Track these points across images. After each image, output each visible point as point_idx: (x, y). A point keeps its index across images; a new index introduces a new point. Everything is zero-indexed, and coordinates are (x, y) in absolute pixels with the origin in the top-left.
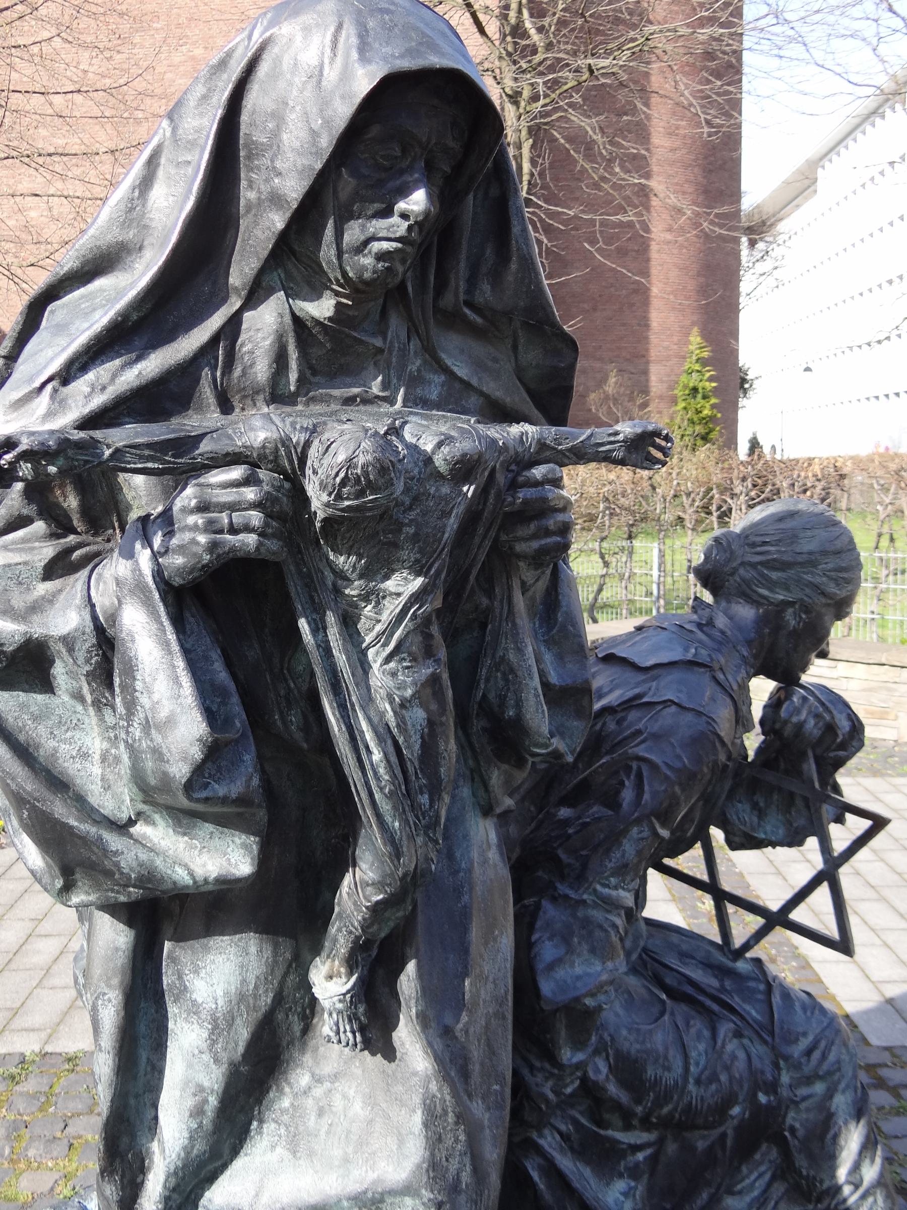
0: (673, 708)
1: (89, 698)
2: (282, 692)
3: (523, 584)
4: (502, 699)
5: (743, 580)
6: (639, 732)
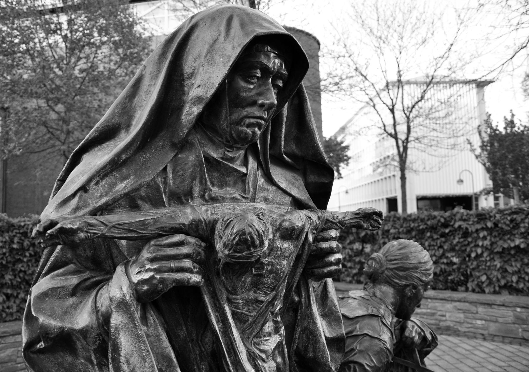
0: (367, 337)
1: (95, 362)
2: (197, 352)
3: (314, 288)
4: (306, 348)
5: (387, 276)
6: (353, 350)
